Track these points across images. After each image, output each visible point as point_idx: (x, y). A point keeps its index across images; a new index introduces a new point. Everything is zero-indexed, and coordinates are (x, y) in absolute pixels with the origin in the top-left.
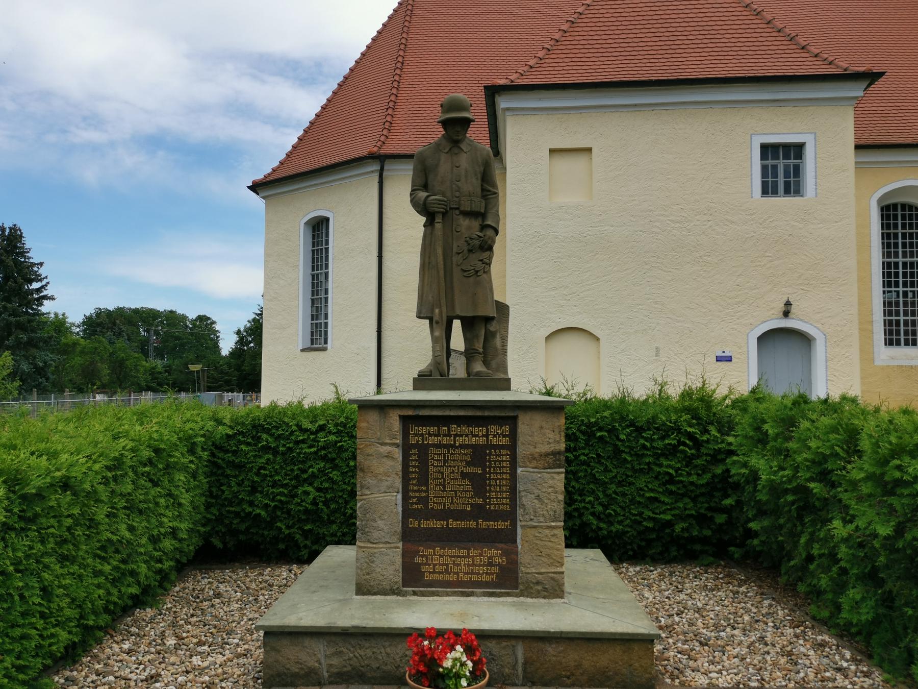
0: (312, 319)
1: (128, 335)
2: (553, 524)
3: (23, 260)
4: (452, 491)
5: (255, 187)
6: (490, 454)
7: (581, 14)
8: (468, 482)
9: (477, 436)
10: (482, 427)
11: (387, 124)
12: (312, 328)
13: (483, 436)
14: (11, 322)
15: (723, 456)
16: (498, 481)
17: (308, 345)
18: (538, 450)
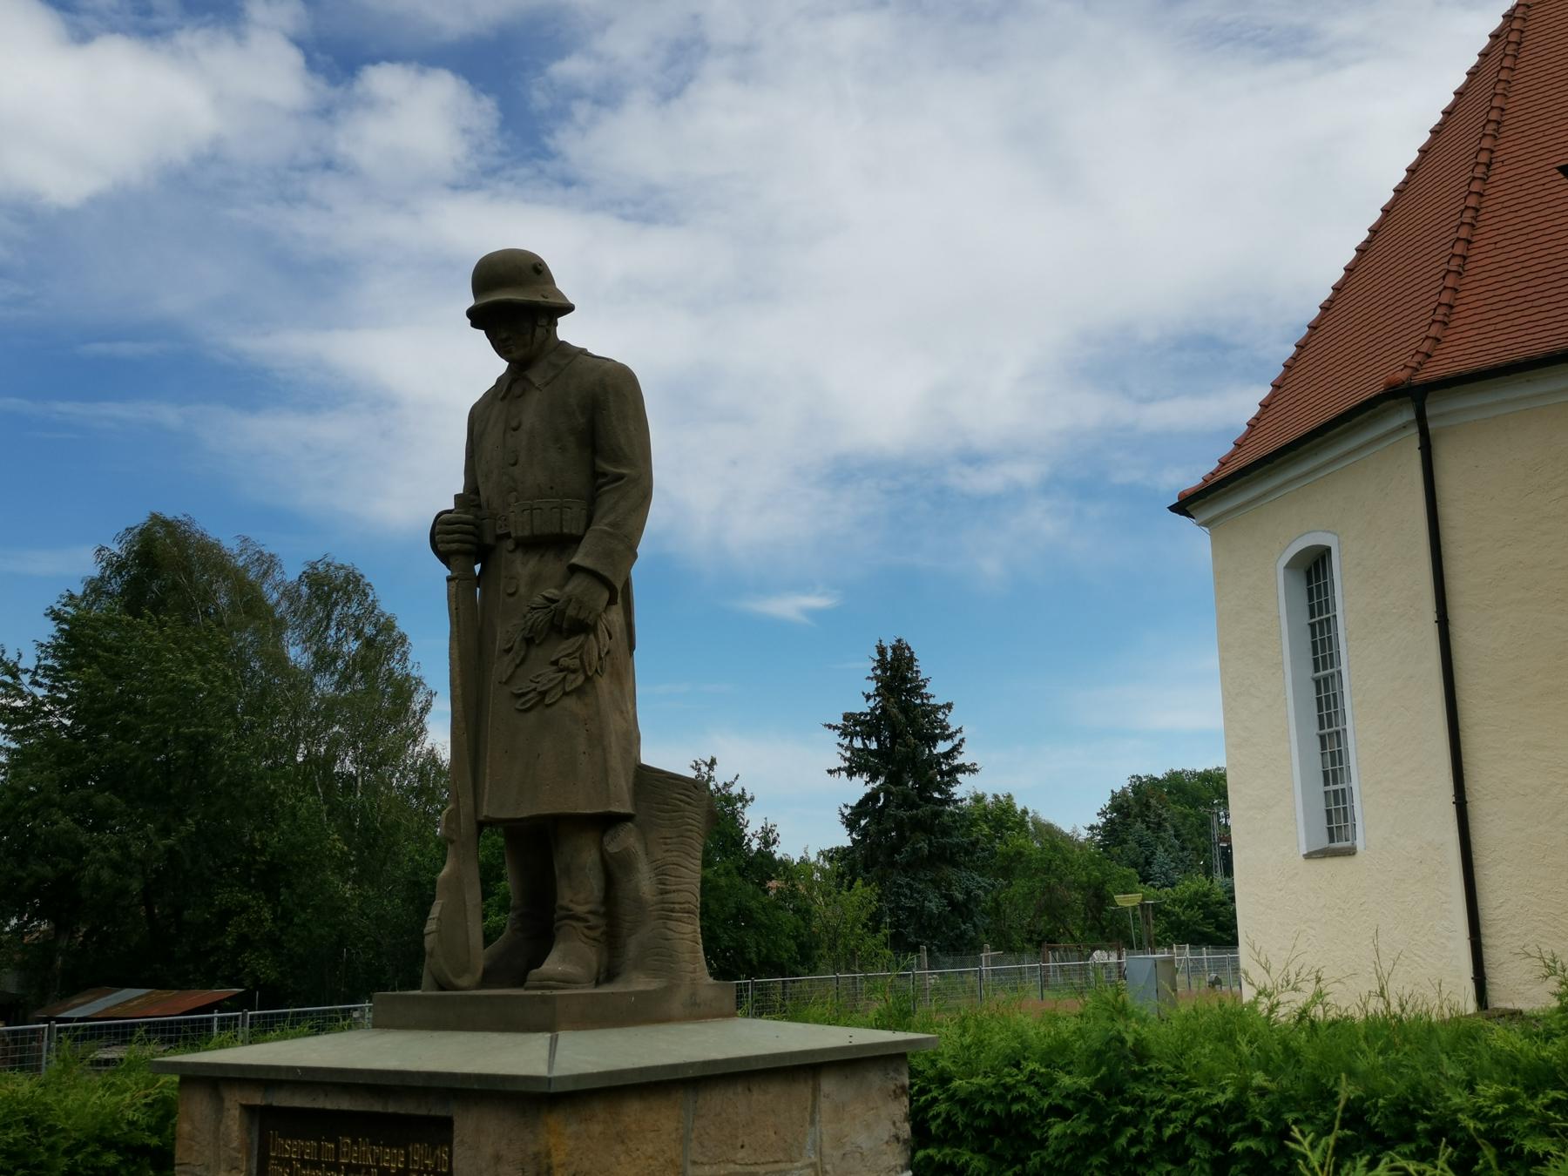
0: (1326, 783)
1: (1174, 826)
3: (918, 701)
5: (1185, 505)
10: (398, 1147)
12: (1327, 804)
17: (1323, 842)
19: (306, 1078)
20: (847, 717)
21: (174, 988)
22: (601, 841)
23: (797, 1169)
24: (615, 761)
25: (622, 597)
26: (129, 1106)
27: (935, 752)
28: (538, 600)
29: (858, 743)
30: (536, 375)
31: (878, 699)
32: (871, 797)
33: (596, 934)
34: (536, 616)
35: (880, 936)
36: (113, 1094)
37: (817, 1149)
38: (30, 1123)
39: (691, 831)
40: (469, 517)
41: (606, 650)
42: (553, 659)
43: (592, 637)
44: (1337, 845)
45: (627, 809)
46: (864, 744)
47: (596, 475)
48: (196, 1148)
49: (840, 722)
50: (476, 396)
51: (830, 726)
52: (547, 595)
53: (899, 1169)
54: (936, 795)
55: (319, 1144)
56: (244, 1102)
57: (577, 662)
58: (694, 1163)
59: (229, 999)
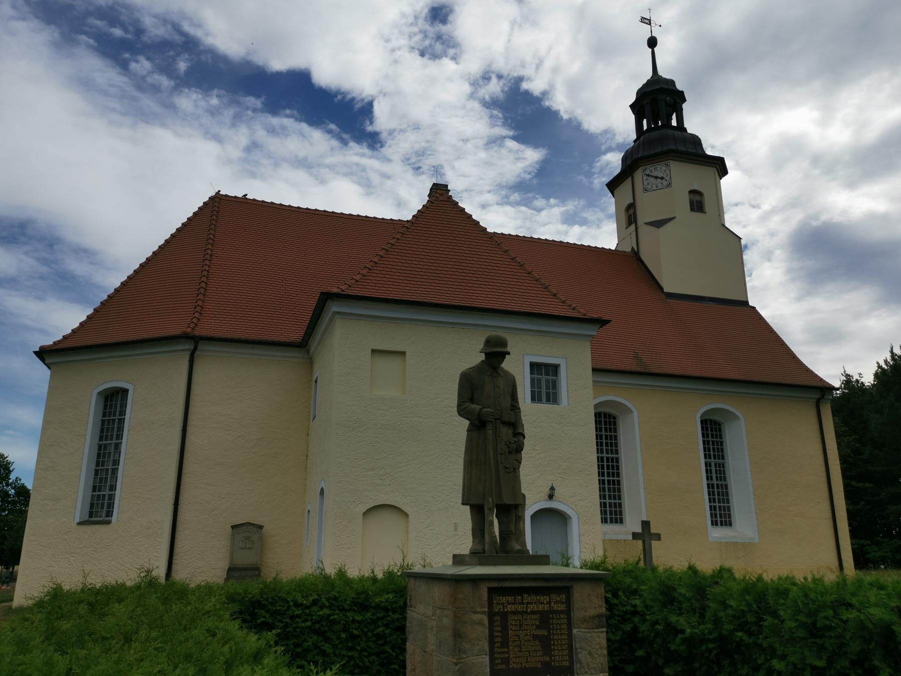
4: (526, 651)
5: (43, 354)
6: (553, 618)
7: (393, 245)
8: (537, 643)
9: (541, 603)
10: (547, 596)
11: (198, 309)
13: (547, 603)
15: (629, 616)
16: (559, 641)
17: (86, 517)
44: (93, 519)
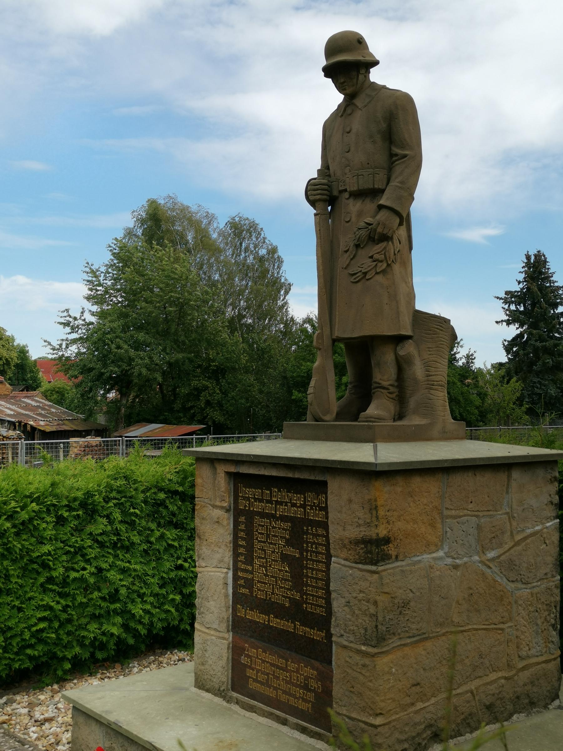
2: (363, 648)
3: (548, 285)
10: (300, 494)
14: (538, 347)
18: (347, 534)
19: (255, 460)
20: (507, 293)
21: (174, 424)
22: (396, 350)
23: (499, 514)
24: (403, 308)
25: (406, 221)
26: (168, 473)
27: (557, 312)
28: (362, 224)
29: (513, 307)
30: (358, 102)
31: (525, 284)
32: (520, 336)
33: (393, 396)
34: (361, 232)
35: (523, 409)
36: (160, 467)
37: (510, 506)
38: (126, 478)
39: (443, 344)
40: (325, 181)
41: (398, 250)
42: (370, 255)
43: (390, 243)
45: (409, 333)
46: (517, 308)
47: (392, 155)
48: (205, 490)
49: (503, 295)
50: (326, 115)
51: (498, 298)
52: (367, 221)
53: (552, 518)
54: (556, 335)
55: (262, 491)
56: (226, 470)
57: (383, 256)
58: (447, 509)
59: (199, 430)
